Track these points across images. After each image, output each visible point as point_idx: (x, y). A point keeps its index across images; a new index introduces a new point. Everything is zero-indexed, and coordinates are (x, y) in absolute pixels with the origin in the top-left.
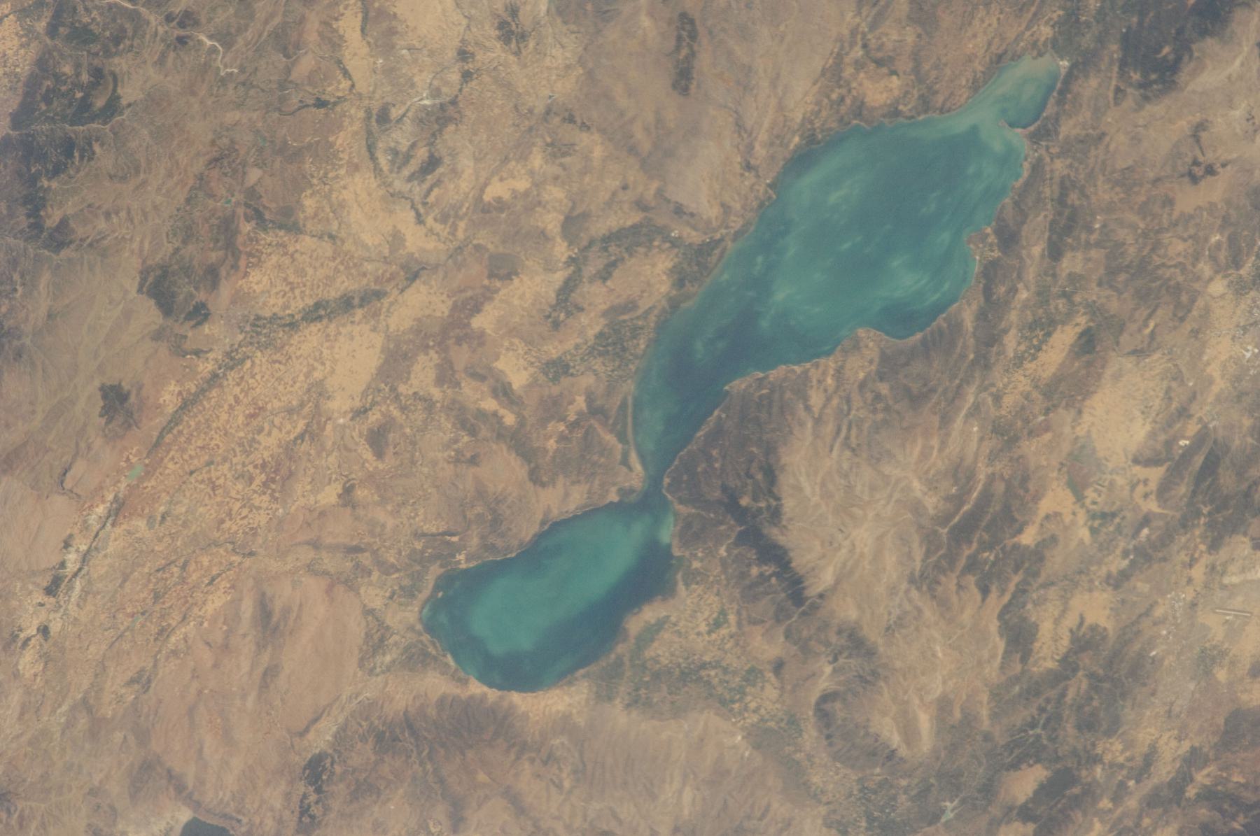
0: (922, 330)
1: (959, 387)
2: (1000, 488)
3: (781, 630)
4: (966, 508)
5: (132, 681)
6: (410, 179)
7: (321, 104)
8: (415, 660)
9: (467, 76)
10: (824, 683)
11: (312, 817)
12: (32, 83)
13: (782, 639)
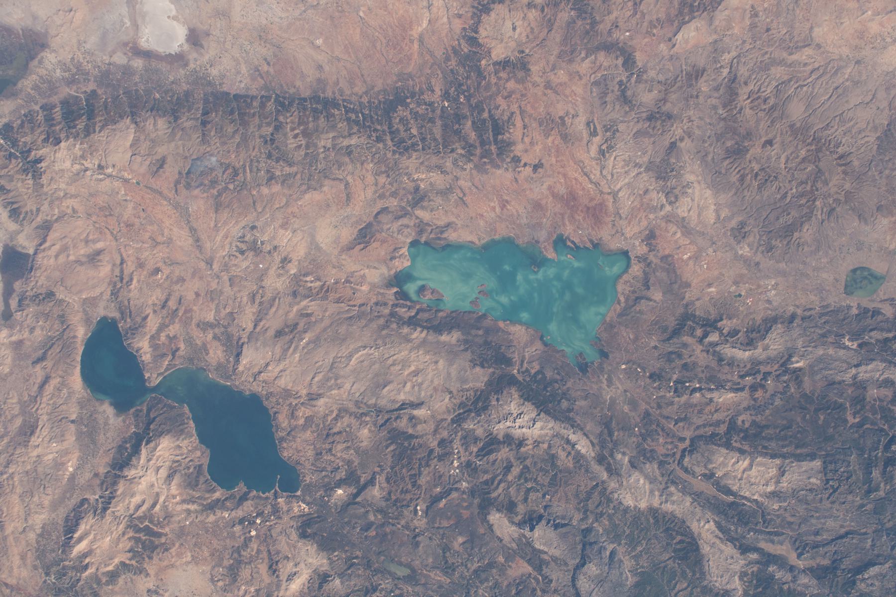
2: (163, 540)
3: (109, 469)
5: (73, 209)
7: (254, 203)
8: (87, 321)
9: (269, 252)
12: (247, 96)
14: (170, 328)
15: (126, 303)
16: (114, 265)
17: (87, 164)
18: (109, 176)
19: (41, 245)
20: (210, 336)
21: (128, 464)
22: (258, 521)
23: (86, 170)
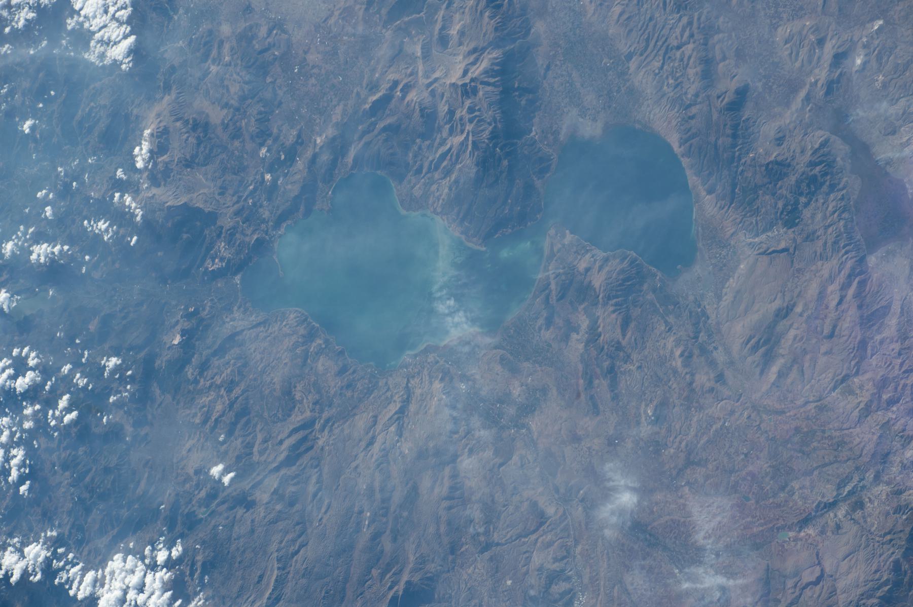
4: (406, 19)
13: (533, 31)
14: (581, 346)
15: (671, 319)
16: (732, 363)
17: (882, 489)
18: (832, 505)
19: (862, 284)
20: (517, 391)
22: (268, 177)
23: (877, 478)
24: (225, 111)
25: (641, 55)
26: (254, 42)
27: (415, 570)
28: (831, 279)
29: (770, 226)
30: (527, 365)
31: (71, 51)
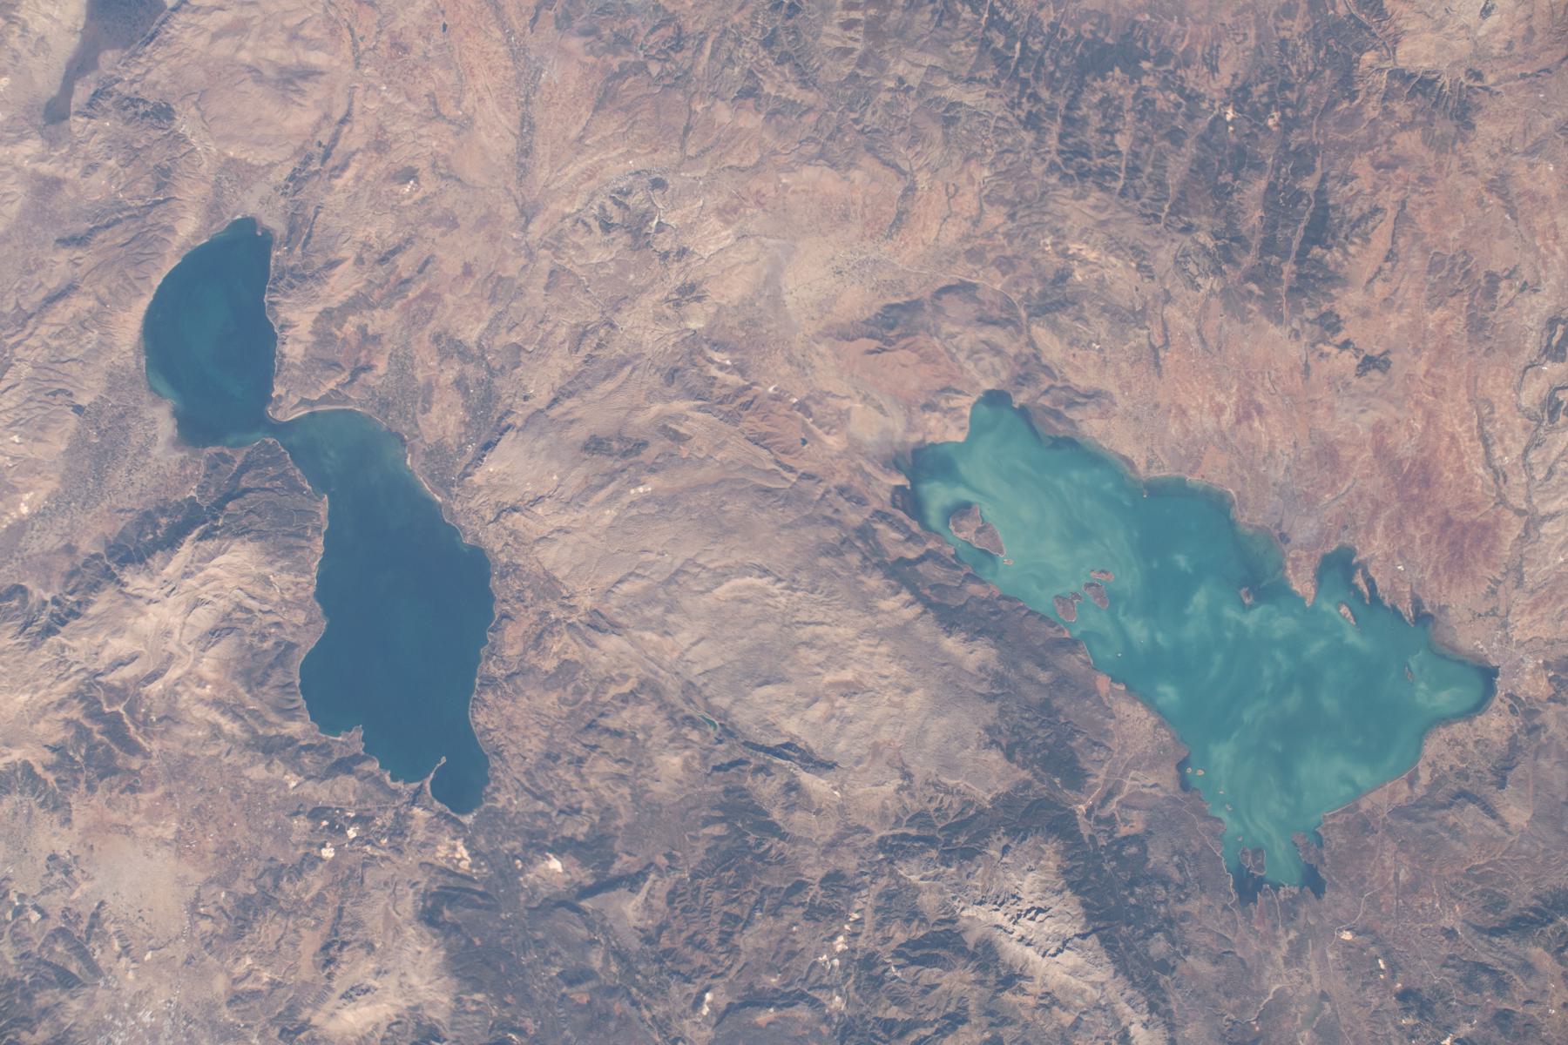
0: (301, 686)
1: (242, 718)
2: (136, 763)
4: (133, 729)
6: (602, 207)
7: (687, 129)
10: (38, 593)
11: (125, 109)
13: (93, 552)
15: (311, 211)
16: (326, 117)
20: (450, 375)
21: (141, 560)
24: (303, 931)
25: (71, 395)
26: (221, 932)
27: (667, 399)
28: (201, 30)
29: (180, 139)
30: (420, 376)
31: (154, 533)
